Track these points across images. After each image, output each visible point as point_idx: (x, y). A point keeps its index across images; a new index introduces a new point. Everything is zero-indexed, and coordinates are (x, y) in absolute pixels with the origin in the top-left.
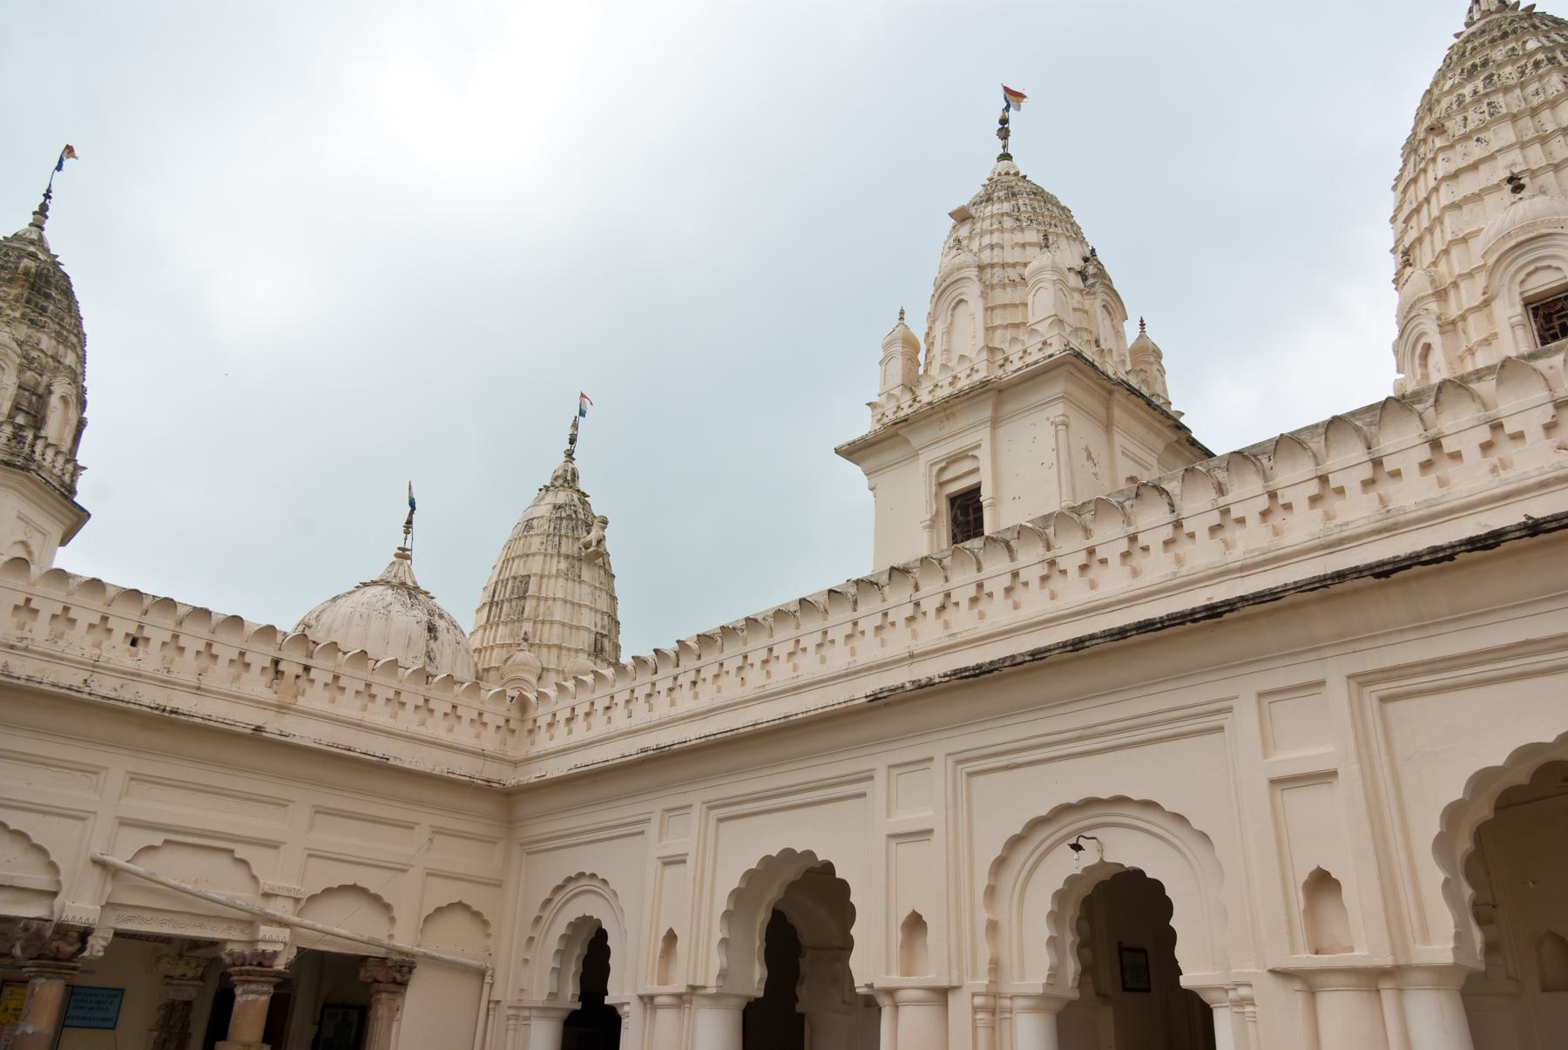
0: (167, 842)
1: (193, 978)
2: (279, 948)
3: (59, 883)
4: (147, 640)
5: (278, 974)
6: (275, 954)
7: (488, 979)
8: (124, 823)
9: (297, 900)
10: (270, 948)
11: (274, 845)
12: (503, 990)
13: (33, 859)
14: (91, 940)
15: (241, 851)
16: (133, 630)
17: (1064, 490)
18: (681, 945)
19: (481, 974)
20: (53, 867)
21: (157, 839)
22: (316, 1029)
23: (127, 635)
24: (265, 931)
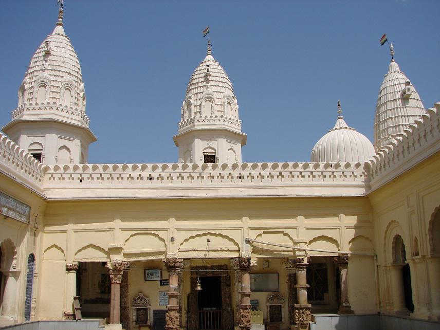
0: (132, 236)
1: (293, 267)
2: (303, 257)
3: (239, 248)
4: (243, 176)
5: (305, 265)
6: (303, 259)
7: (375, 258)
8: (251, 229)
9: (306, 243)
10: (301, 258)
11: (295, 228)
12: (381, 261)
13: (226, 240)
14: (251, 261)
15: (286, 231)
16: (238, 175)
17: (231, 128)
18: (37, 258)
19: (373, 257)
20: (237, 244)
21: (261, 232)
22: (335, 278)
23: (148, 178)
24: (298, 253)
